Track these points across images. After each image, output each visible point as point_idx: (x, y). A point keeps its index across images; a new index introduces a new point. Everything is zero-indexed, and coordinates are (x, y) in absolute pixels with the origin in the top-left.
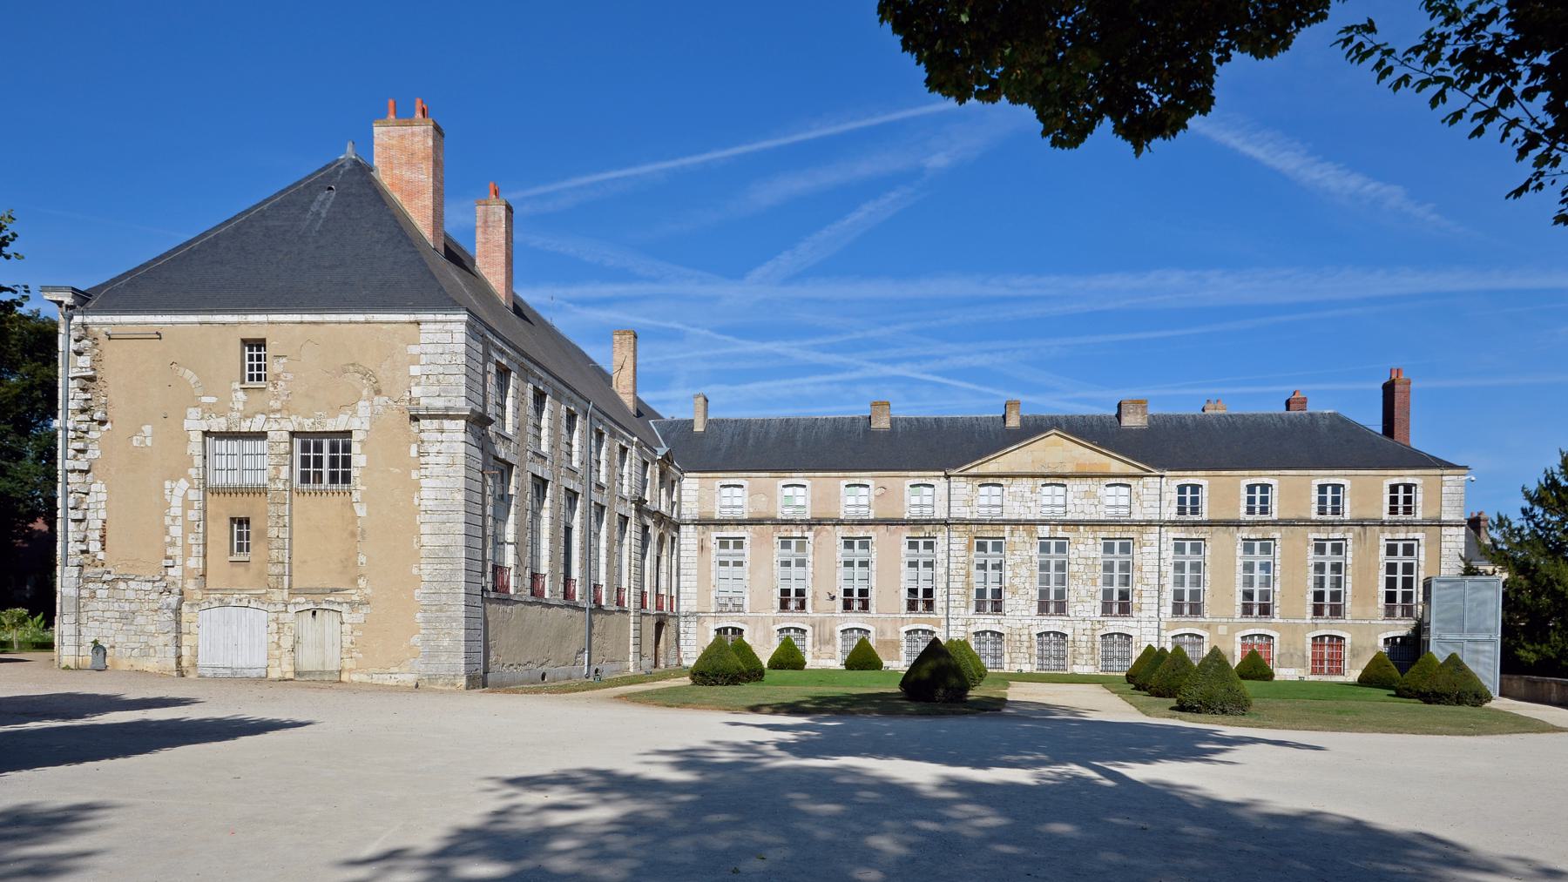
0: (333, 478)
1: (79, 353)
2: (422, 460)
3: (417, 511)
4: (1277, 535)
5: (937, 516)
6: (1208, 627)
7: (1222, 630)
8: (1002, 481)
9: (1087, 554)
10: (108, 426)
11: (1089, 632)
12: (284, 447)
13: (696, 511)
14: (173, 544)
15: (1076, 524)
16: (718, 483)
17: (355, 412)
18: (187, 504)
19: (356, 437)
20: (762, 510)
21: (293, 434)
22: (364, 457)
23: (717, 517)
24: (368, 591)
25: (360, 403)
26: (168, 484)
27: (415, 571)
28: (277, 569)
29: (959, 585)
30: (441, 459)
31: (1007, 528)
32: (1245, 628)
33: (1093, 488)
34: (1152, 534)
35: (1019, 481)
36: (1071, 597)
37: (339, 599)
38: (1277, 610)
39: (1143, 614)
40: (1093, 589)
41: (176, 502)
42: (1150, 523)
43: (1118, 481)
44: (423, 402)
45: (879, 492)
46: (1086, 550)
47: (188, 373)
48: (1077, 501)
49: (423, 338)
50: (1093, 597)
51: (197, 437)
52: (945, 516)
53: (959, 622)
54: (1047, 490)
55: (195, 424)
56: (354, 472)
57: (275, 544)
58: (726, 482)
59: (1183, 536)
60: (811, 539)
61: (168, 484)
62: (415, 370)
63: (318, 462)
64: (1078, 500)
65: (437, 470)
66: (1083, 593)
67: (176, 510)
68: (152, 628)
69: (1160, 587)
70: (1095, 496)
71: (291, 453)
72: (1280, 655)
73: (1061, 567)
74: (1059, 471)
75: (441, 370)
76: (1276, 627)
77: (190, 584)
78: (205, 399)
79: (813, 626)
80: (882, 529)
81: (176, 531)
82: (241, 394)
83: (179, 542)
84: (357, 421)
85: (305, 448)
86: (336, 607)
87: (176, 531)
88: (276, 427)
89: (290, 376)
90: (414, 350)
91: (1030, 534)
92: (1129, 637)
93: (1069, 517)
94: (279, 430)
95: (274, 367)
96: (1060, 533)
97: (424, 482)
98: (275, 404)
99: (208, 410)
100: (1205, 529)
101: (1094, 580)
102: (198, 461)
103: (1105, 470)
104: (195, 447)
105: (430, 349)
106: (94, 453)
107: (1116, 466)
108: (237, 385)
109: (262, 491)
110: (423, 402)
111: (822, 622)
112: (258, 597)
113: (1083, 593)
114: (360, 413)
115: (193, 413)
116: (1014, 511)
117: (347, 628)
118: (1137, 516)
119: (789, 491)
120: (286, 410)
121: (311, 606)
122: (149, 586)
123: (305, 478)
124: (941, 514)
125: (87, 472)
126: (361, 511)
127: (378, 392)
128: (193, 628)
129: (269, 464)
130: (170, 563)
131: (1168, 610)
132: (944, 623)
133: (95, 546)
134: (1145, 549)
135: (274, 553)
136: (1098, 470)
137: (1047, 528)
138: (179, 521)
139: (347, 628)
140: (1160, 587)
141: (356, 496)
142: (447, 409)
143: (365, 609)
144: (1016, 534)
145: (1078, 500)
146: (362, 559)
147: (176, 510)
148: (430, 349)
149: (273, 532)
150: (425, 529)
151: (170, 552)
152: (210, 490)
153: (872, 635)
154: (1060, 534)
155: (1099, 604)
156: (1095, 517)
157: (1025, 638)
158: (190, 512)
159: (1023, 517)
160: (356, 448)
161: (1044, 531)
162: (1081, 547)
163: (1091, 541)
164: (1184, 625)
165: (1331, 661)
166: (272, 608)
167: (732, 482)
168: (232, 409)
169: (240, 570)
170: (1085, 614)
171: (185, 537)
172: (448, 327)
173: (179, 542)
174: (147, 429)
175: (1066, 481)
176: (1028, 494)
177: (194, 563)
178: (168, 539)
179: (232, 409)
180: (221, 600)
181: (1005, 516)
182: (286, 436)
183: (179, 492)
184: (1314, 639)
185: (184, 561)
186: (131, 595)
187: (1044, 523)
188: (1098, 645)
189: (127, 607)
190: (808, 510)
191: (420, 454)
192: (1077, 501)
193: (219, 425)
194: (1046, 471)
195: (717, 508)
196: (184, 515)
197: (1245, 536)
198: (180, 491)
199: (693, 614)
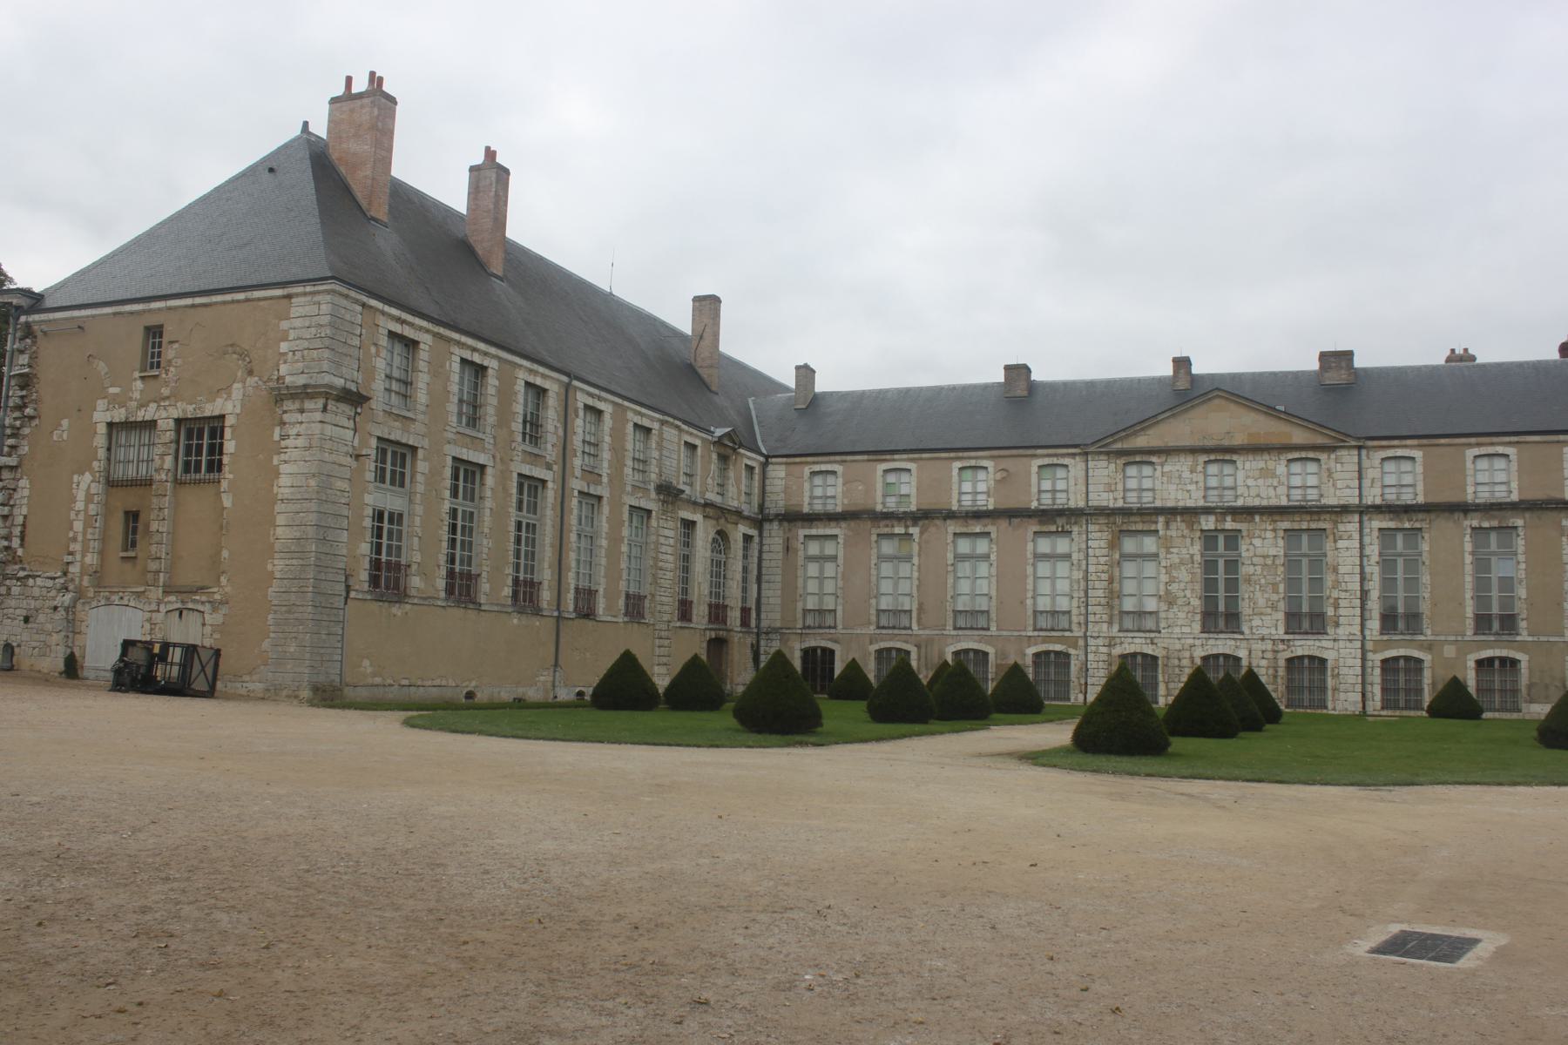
0: (210, 469)
1: (21, 352)
2: (283, 443)
3: (274, 500)
4: (1519, 522)
5: (1072, 504)
6: (1429, 647)
7: (1449, 651)
8: (1154, 459)
9: (1264, 551)
10: (37, 422)
11: (1269, 655)
12: (170, 435)
13: (781, 503)
14: (74, 539)
15: (1248, 512)
16: (807, 470)
17: (229, 397)
18: (89, 498)
19: (229, 421)
20: (859, 501)
21: (178, 421)
22: (233, 443)
23: (806, 510)
24: (228, 589)
25: (236, 385)
26: (76, 478)
27: (270, 567)
28: (153, 566)
29: (1100, 593)
30: (300, 442)
31: (1161, 519)
32: (1479, 649)
33: (1271, 464)
34: (1351, 526)
35: (1173, 459)
36: (1245, 608)
37: (204, 598)
38: (1523, 624)
39: (1340, 631)
40: (1275, 597)
41: (81, 495)
42: (1345, 510)
43: (1303, 455)
44: (288, 380)
45: (999, 476)
46: (1263, 547)
47: (102, 364)
48: (1250, 482)
49: (294, 312)
50: (1274, 608)
51: (102, 429)
52: (1081, 504)
53: (1100, 642)
54: (1296, 468)
55: (102, 415)
56: (226, 460)
57: (156, 538)
58: (817, 468)
59: (1392, 525)
60: (916, 537)
61: (76, 478)
62: (284, 347)
63: (200, 447)
64: (1252, 482)
65: (295, 454)
66: (1261, 602)
67: (80, 505)
68: (49, 627)
69: (1364, 595)
70: (1274, 475)
71: (178, 442)
72: (1530, 686)
73: (1232, 565)
74: (1226, 443)
75: (306, 344)
76: (1523, 647)
77: (86, 581)
78: (112, 390)
79: (918, 646)
80: (1004, 523)
81: (78, 526)
82: (139, 384)
83: (80, 538)
84: (229, 406)
85: (189, 437)
86: (200, 608)
87: (78, 526)
88: (164, 414)
89: (180, 362)
90: (284, 325)
91: (1191, 526)
92: (1323, 661)
93: (1240, 503)
94: (165, 417)
95: (169, 353)
96: (1229, 524)
97: (284, 468)
98: (165, 391)
99: (115, 402)
100: (1420, 516)
101: (1275, 586)
102: (102, 453)
103: (1285, 441)
104: (100, 441)
105: (298, 323)
106: (24, 450)
107: (1299, 436)
108: (137, 374)
109: (147, 483)
110: (288, 380)
111: (930, 641)
112: (139, 595)
113: (1261, 602)
114: (234, 396)
115: (101, 404)
116: (1173, 496)
117: (208, 629)
118: (1330, 500)
119: (891, 478)
120: (175, 396)
121: (179, 605)
122: (50, 583)
123: (187, 469)
124: (1077, 501)
125: (16, 467)
126: (227, 501)
127: (250, 373)
128: (83, 629)
129: (162, 460)
130: (70, 558)
131: (1374, 624)
132: (1081, 642)
133: (16, 543)
134: (1341, 544)
135: (154, 548)
136: (1275, 441)
137: (1212, 518)
138: (81, 517)
139: (208, 629)
140: (1364, 595)
141: (224, 485)
142: (305, 386)
143: (224, 610)
144: (1173, 526)
145: (1252, 482)
146: (225, 554)
147: (80, 505)
148: (298, 323)
149: (154, 526)
150: (280, 520)
151: (72, 547)
152: (111, 484)
153: (914, 656)
154: (1229, 524)
155: (1281, 616)
156: (1274, 502)
157: (1186, 662)
158: (91, 506)
159: (1181, 504)
160: (228, 433)
161: (1209, 523)
162: (1257, 542)
163: (1269, 535)
164: (1397, 645)
165: (1408, 691)
166: (147, 608)
167: (824, 467)
168: (131, 399)
169: (128, 566)
170: (1265, 632)
171: (84, 533)
172: (317, 298)
173: (80, 538)
174: (65, 423)
175: (1235, 457)
176: (1186, 474)
177: (91, 559)
178: (71, 534)
179: (131, 399)
180: (108, 599)
181: (1158, 504)
182: (172, 423)
183: (83, 486)
184: (1479, 663)
185: (83, 556)
186: (36, 592)
187: (1207, 511)
188: (1282, 672)
189: (33, 604)
190: (913, 500)
191: (284, 437)
192: (1250, 482)
193: (119, 415)
194: (1209, 443)
195: (807, 500)
196: (86, 510)
197: (1475, 523)
198: (86, 484)
199: (776, 630)
